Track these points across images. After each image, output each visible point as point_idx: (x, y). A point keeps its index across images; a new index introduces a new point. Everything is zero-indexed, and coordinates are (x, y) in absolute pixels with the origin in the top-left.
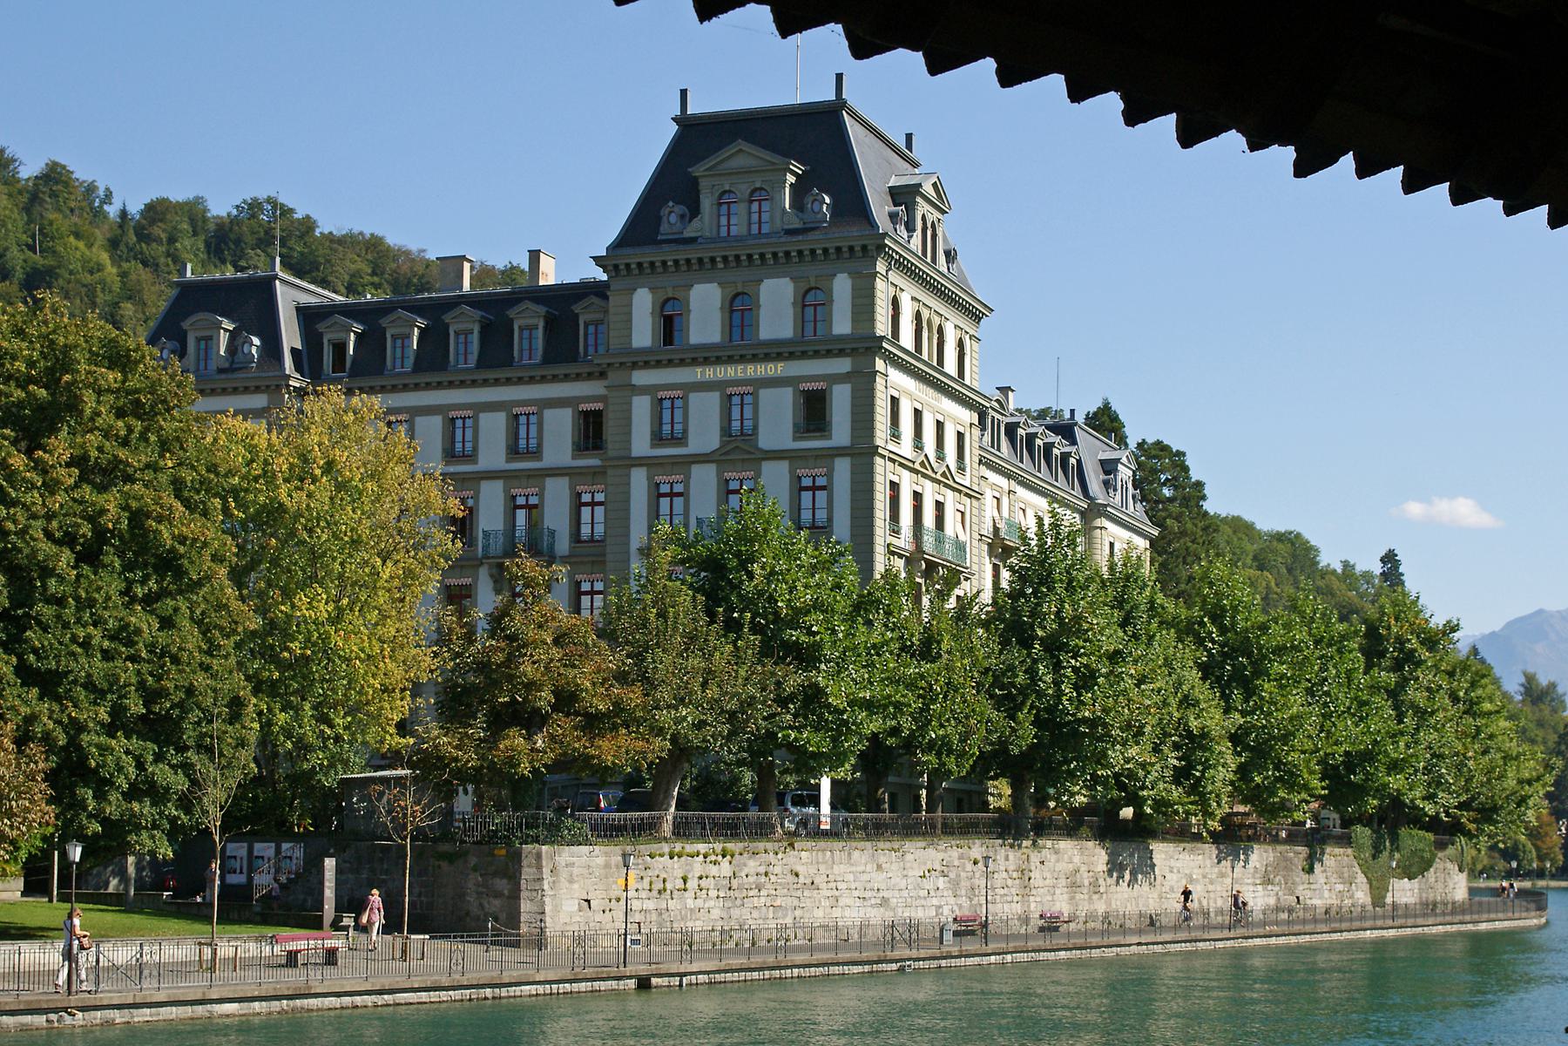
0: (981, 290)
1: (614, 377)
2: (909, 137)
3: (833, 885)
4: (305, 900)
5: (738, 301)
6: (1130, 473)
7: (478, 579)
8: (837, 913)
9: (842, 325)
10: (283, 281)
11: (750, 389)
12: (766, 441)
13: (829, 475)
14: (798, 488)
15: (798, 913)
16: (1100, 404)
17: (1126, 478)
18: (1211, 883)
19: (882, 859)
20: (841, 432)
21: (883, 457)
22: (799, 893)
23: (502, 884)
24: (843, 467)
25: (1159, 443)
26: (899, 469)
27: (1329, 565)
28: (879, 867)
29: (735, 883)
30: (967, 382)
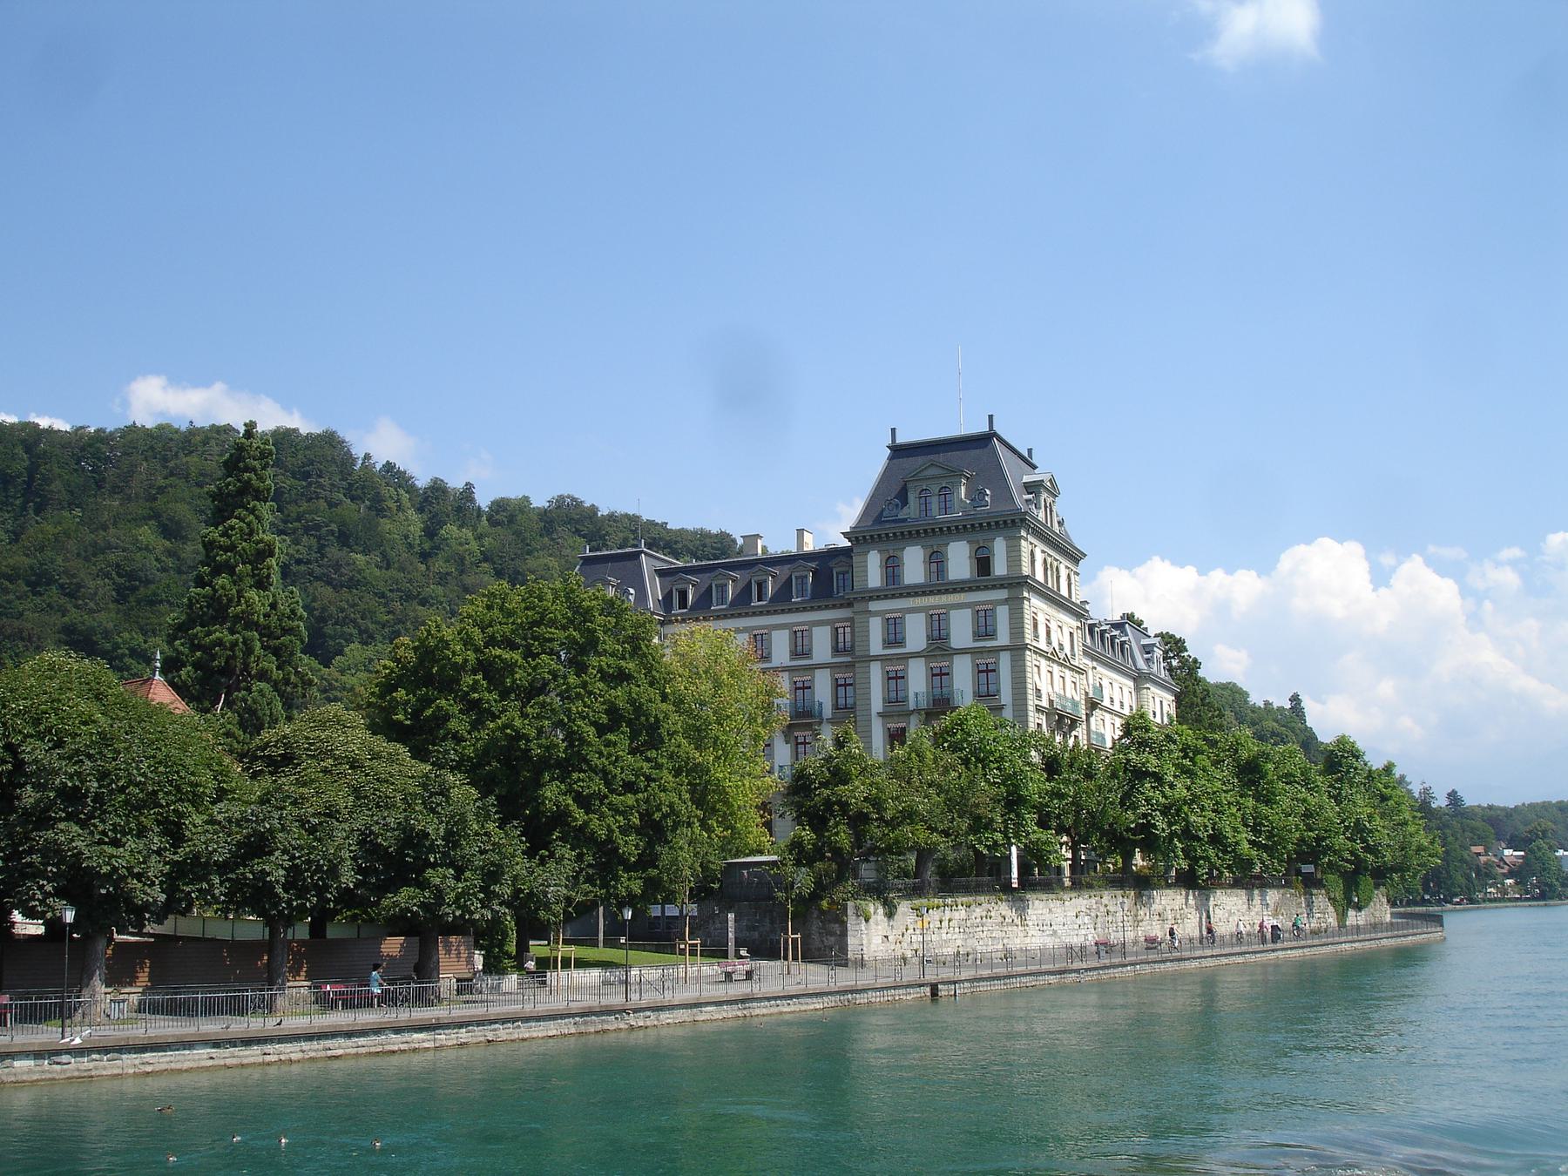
0: (1079, 542)
1: (858, 607)
2: (1030, 451)
5: (890, 561)
7: (910, 723)
8: (1028, 940)
10: (646, 554)
11: (807, 627)
14: (837, 685)
15: (1005, 941)
17: (1159, 656)
20: (1003, 638)
21: (1030, 650)
23: (836, 927)
26: (1039, 658)
30: (1073, 600)
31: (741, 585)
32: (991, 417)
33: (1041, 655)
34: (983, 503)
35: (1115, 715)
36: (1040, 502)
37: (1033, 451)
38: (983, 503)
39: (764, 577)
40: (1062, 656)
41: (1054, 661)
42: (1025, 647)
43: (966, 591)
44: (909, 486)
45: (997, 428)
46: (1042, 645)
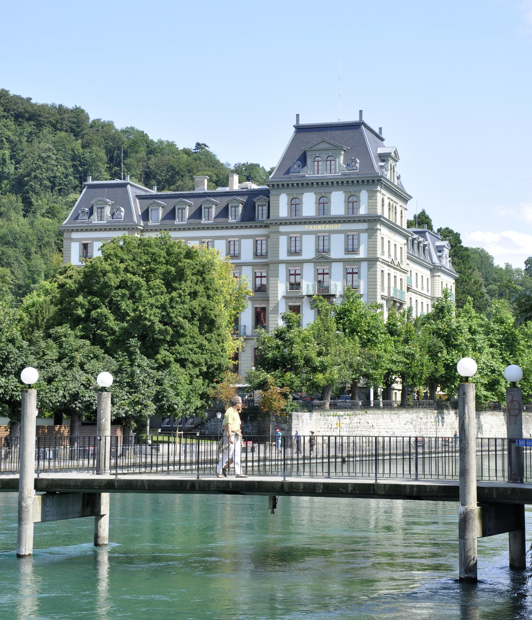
1: (272, 229)
2: (380, 129)
3: (378, 427)
4: (205, 432)
6: (448, 251)
9: (363, 211)
10: (131, 185)
12: (333, 255)
13: (359, 268)
16: (421, 211)
18: (499, 428)
19: (393, 417)
20: (362, 253)
21: (380, 261)
22: (369, 430)
24: (364, 266)
25: (447, 229)
27: (498, 265)
28: (392, 420)
29: (351, 425)
31: (194, 209)
32: (361, 112)
33: (385, 264)
34: (355, 168)
35: (419, 294)
36: (388, 167)
37: (383, 129)
38: (355, 168)
39: (210, 205)
40: (396, 263)
41: (391, 267)
42: (376, 260)
43: (342, 223)
44: (308, 154)
45: (365, 119)
46: (386, 257)
